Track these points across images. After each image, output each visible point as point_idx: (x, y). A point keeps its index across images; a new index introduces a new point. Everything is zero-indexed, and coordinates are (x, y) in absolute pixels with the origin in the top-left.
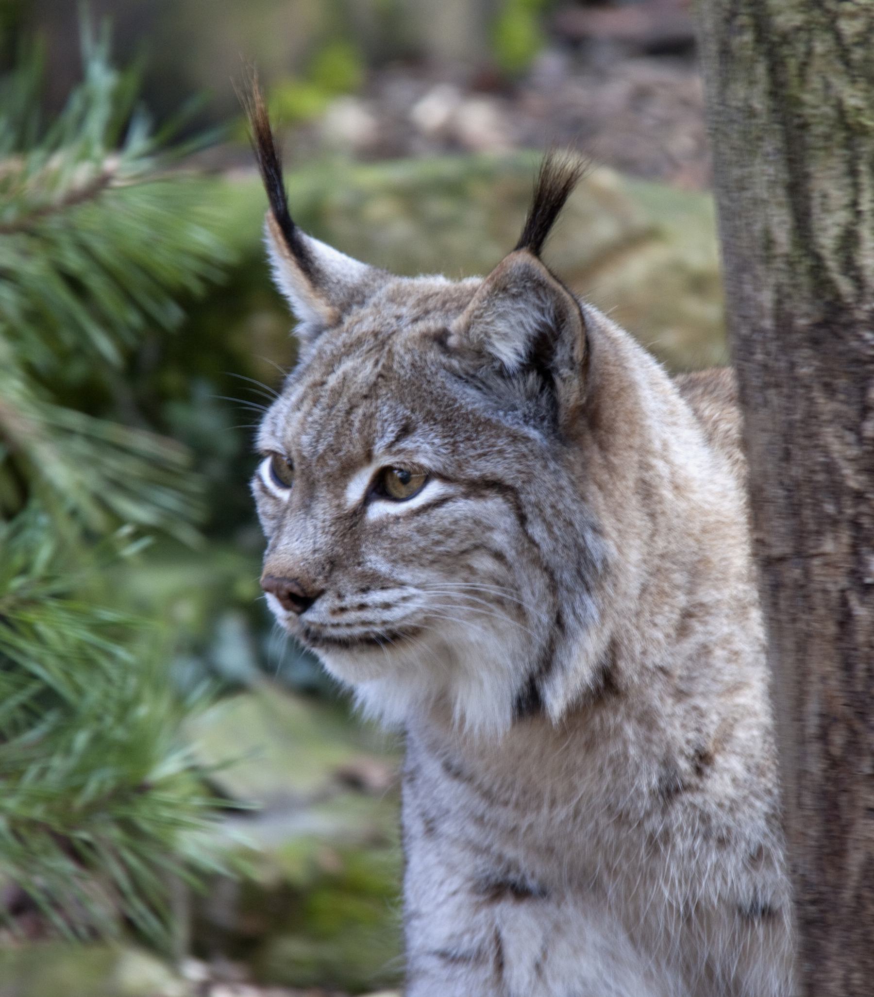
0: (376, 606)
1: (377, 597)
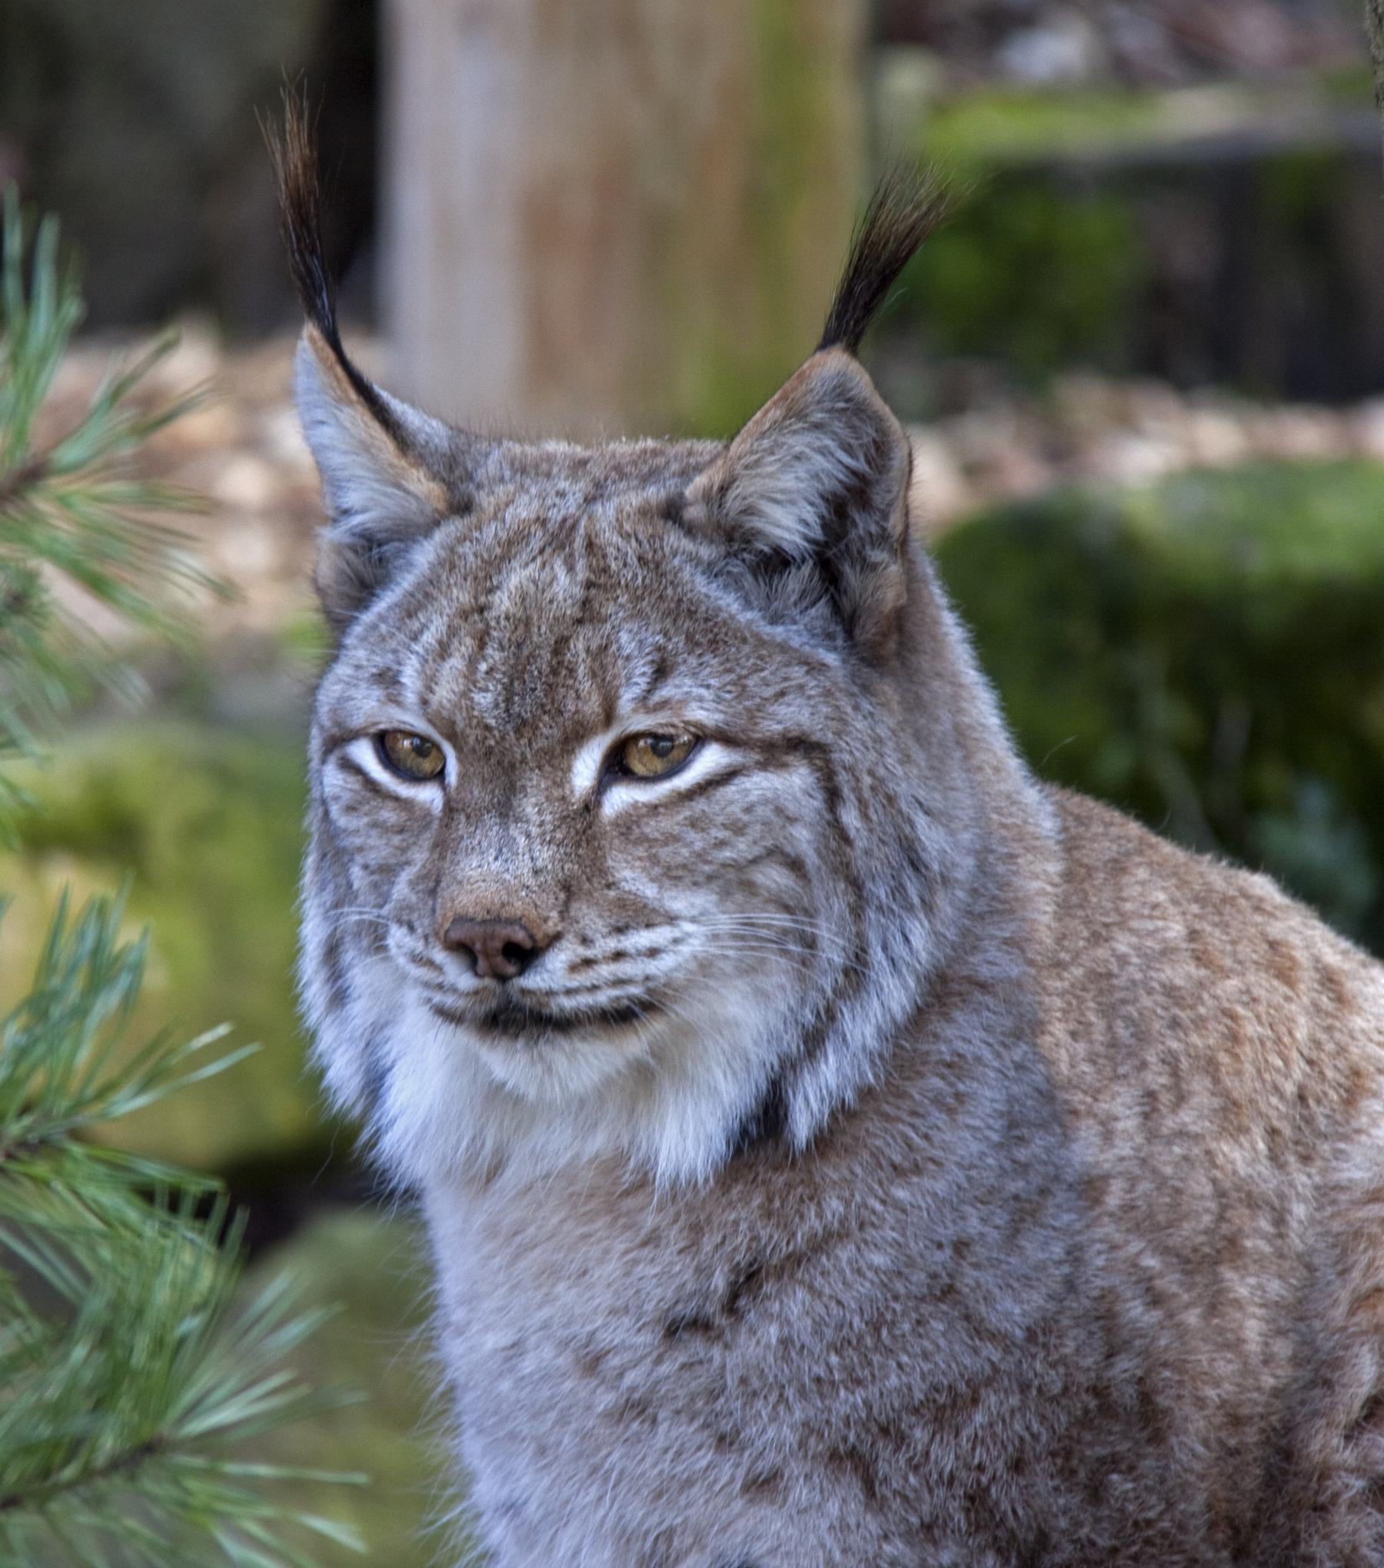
0: (639, 953)
1: (641, 939)
